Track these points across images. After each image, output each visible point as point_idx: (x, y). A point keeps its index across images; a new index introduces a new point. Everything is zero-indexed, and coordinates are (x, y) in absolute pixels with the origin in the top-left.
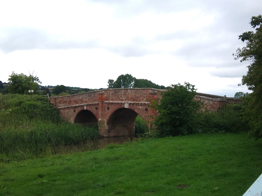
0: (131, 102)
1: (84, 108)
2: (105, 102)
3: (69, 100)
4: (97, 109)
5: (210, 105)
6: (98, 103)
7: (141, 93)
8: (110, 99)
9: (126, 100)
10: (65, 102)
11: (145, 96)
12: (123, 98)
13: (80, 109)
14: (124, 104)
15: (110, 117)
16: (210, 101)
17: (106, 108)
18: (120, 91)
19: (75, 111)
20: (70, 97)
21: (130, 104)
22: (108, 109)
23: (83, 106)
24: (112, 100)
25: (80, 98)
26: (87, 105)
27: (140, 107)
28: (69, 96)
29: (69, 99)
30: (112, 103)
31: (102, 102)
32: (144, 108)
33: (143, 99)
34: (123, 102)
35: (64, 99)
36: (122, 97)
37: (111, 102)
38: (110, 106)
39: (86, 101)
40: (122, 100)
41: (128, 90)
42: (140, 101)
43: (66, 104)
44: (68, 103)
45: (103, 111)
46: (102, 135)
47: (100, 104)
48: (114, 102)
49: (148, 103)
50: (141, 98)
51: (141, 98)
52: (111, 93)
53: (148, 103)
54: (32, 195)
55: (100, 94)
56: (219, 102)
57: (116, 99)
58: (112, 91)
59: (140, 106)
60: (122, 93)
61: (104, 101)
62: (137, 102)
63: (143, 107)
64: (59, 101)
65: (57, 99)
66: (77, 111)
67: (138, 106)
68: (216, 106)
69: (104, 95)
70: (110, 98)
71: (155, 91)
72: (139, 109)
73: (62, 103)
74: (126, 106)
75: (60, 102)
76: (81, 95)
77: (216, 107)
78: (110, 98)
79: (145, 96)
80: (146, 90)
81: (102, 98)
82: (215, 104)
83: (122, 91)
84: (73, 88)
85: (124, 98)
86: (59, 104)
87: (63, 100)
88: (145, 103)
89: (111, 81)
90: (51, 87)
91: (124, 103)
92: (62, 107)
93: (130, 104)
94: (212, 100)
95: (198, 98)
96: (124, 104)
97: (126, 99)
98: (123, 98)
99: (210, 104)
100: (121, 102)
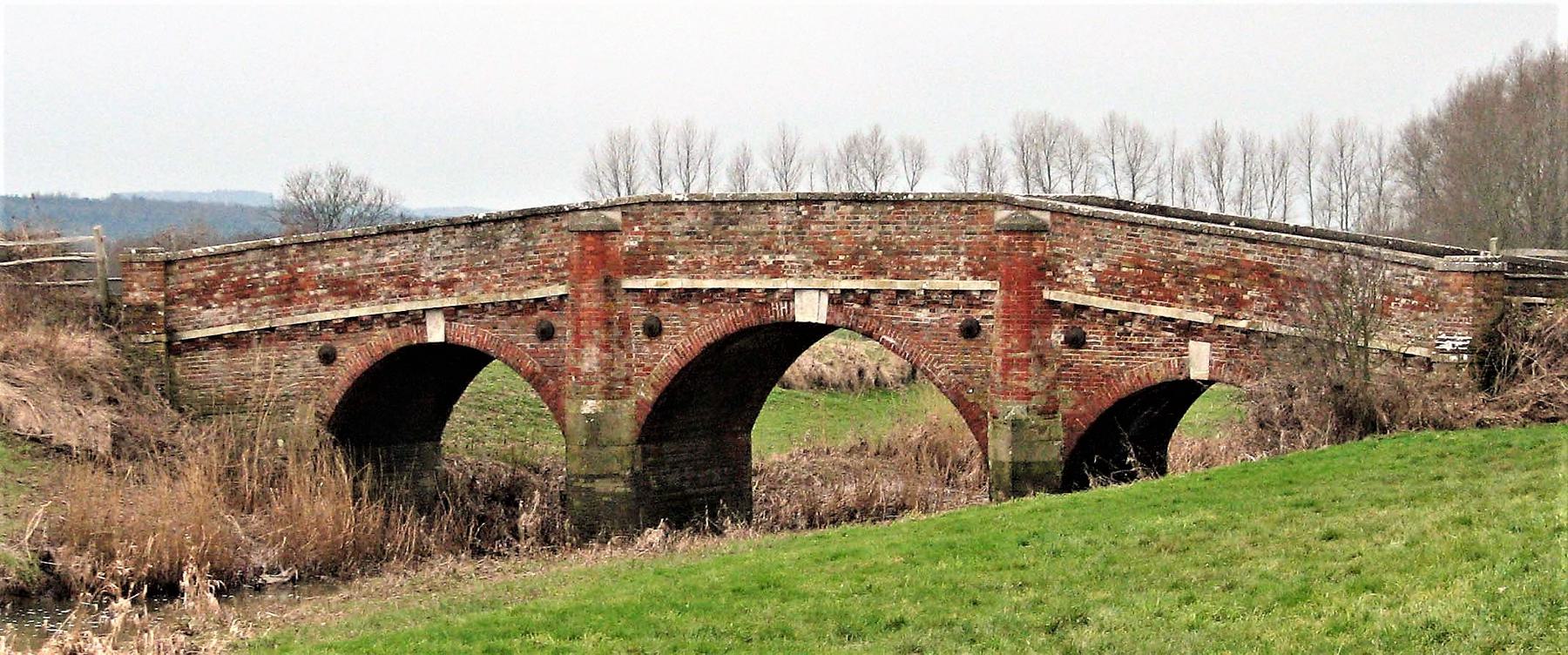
1: (424, 332)
2: (629, 283)
3: (276, 274)
5: (1410, 292)
6: (561, 290)
7: (928, 222)
8: (671, 263)
9: (808, 268)
10: (243, 290)
11: (957, 245)
12: (781, 258)
13: (384, 340)
14: (789, 296)
15: (668, 388)
16: (1410, 271)
17: (637, 328)
18: (761, 208)
19: (328, 357)
20: (292, 251)
23: (418, 319)
24: (694, 269)
25: (386, 259)
26: (451, 314)
27: (923, 315)
28: (282, 246)
29: (279, 266)
30: (1307, 236)
32: (957, 318)
33: (944, 266)
34: (783, 284)
35: (240, 269)
36: (780, 253)
37: (678, 283)
38: (671, 317)
39: (447, 286)
40: (775, 271)
41: (829, 205)
42: (920, 273)
43: (257, 306)
44: (273, 297)
45: (614, 347)
46: (1010, 434)
49: (986, 285)
50: (933, 259)
51: (933, 259)
52: (679, 224)
53: (986, 285)
54: (1219, 654)
55: (583, 233)
56: (1475, 273)
57: (723, 266)
58: (686, 209)
59: (923, 306)
60: (779, 228)
61: (618, 283)
62: (900, 285)
63: (943, 313)
64: (190, 285)
65: (176, 268)
66: (354, 358)
67: (904, 310)
68: (1453, 294)
69: (617, 235)
70: (671, 258)
71: (1033, 213)
72: (915, 328)
73: (216, 295)
75: (203, 295)
76: (395, 238)
77: (1452, 300)
78: (671, 258)
79: (957, 245)
80: (964, 208)
81: (602, 256)
82: (1447, 285)
83: (779, 208)
85: (792, 257)
86: (193, 309)
87: (224, 274)
88: (963, 286)
91: (794, 290)
92: (225, 330)
94: (1423, 268)
95: (1329, 252)
96: (789, 296)
97: (811, 261)
98: (781, 258)
99: (1412, 288)
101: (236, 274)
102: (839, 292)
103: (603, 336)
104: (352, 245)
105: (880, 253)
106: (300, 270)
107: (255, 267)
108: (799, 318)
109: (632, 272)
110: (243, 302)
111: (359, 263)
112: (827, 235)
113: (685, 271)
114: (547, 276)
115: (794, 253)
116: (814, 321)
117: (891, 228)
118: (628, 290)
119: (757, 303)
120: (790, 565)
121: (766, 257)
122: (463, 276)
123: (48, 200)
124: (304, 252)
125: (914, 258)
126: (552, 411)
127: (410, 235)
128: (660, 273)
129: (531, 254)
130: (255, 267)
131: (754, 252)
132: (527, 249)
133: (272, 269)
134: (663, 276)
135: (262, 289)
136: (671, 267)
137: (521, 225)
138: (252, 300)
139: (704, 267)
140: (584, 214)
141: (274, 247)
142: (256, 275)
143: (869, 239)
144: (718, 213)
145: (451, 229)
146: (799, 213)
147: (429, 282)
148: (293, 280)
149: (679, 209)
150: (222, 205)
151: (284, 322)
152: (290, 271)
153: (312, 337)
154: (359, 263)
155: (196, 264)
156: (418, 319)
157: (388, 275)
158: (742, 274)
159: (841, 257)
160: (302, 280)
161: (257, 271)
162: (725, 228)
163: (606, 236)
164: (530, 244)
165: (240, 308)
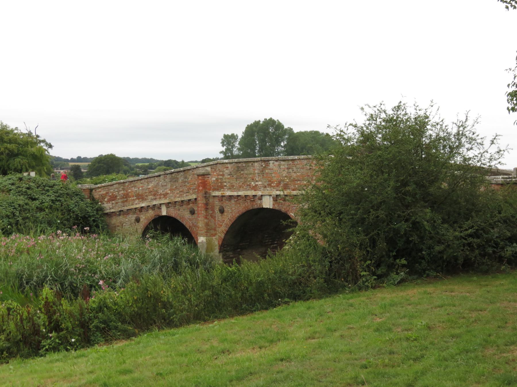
0: (278, 193)
3: (122, 192)
4: (192, 212)
6: (194, 196)
9: (265, 187)
12: (257, 183)
17: (217, 210)
18: (250, 164)
19: (138, 220)
20: (127, 184)
21: (276, 198)
22: (222, 211)
23: (159, 207)
26: (168, 205)
28: (124, 183)
29: (124, 189)
30: (231, 197)
31: (207, 196)
34: (259, 193)
36: (257, 181)
37: (228, 193)
39: (165, 195)
40: (255, 188)
43: (117, 203)
47: (201, 202)
48: (235, 194)
52: (227, 171)
60: (256, 171)
74: (267, 203)
84: (137, 160)
89: (228, 140)
90: (85, 160)
93: (276, 198)
96: (261, 198)
97: (266, 184)
98: (257, 183)
100: (253, 193)
101: (111, 193)
102: (275, 196)
103: (205, 213)
104: (142, 182)
105: (287, 180)
106: (129, 191)
107: (116, 190)
108: (264, 206)
109: (215, 190)
110: (113, 202)
111: (144, 188)
112: (271, 174)
113: (229, 189)
114: (191, 191)
115: (261, 181)
116: (268, 207)
117: (291, 170)
118: (214, 196)
119: (251, 201)
120: (413, 176)
121: (253, 183)
122: (169, 192)
123: (134, 159)
124: (131, 184)
125: (299, 182)
126: (78, 295)
127: (156, 178)
128: (222, 190)
129: (187, 184)
130: (116, 190)
131: (249, 181)
132: (186, 182)
133: (121, 191)
134: (223, 191)
135: (118, 197)
136: (225, 188)
137: (184, 173)
138: (116, 201)
139: (235, 187)
140: (200, 168)
141: (121, 183)
142: (117, 193)
143: (284, 175)
144: (238, 167)
145: (166, 175)
146: (262, 166)
147: (161, 194)
148: (127, 194)
149: (227, 166)
150: (307, 131)
151: (126, 208)
152: (126, 191)
153: (134, 213)
154: (144, 188)
155: (100, 190)
156: (159, 207)
157: (150, 192)
158: (246, 190)
159: (275, 183)
160: (130, 194)
161: (117, 191)
162: (240, 172)
163: (205, 177)
164: (186, 180)
165: (113, 204)
